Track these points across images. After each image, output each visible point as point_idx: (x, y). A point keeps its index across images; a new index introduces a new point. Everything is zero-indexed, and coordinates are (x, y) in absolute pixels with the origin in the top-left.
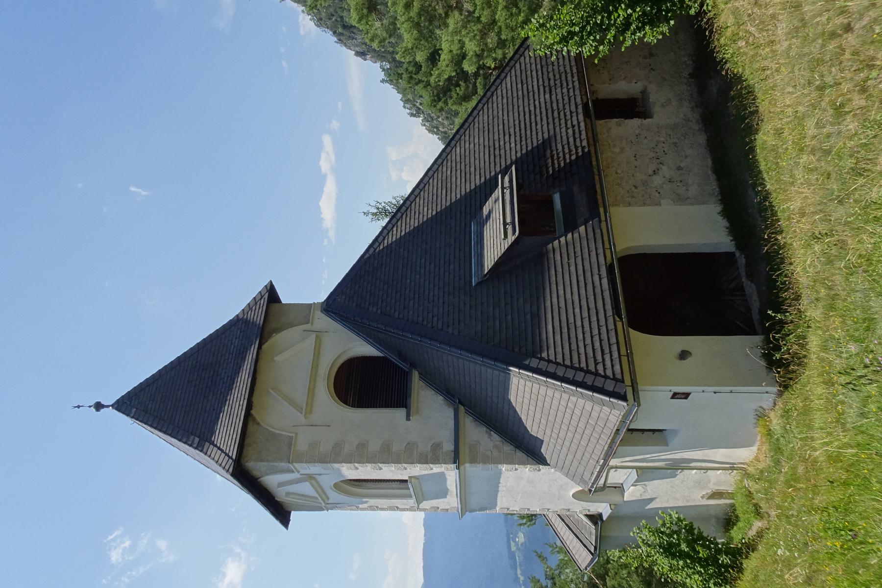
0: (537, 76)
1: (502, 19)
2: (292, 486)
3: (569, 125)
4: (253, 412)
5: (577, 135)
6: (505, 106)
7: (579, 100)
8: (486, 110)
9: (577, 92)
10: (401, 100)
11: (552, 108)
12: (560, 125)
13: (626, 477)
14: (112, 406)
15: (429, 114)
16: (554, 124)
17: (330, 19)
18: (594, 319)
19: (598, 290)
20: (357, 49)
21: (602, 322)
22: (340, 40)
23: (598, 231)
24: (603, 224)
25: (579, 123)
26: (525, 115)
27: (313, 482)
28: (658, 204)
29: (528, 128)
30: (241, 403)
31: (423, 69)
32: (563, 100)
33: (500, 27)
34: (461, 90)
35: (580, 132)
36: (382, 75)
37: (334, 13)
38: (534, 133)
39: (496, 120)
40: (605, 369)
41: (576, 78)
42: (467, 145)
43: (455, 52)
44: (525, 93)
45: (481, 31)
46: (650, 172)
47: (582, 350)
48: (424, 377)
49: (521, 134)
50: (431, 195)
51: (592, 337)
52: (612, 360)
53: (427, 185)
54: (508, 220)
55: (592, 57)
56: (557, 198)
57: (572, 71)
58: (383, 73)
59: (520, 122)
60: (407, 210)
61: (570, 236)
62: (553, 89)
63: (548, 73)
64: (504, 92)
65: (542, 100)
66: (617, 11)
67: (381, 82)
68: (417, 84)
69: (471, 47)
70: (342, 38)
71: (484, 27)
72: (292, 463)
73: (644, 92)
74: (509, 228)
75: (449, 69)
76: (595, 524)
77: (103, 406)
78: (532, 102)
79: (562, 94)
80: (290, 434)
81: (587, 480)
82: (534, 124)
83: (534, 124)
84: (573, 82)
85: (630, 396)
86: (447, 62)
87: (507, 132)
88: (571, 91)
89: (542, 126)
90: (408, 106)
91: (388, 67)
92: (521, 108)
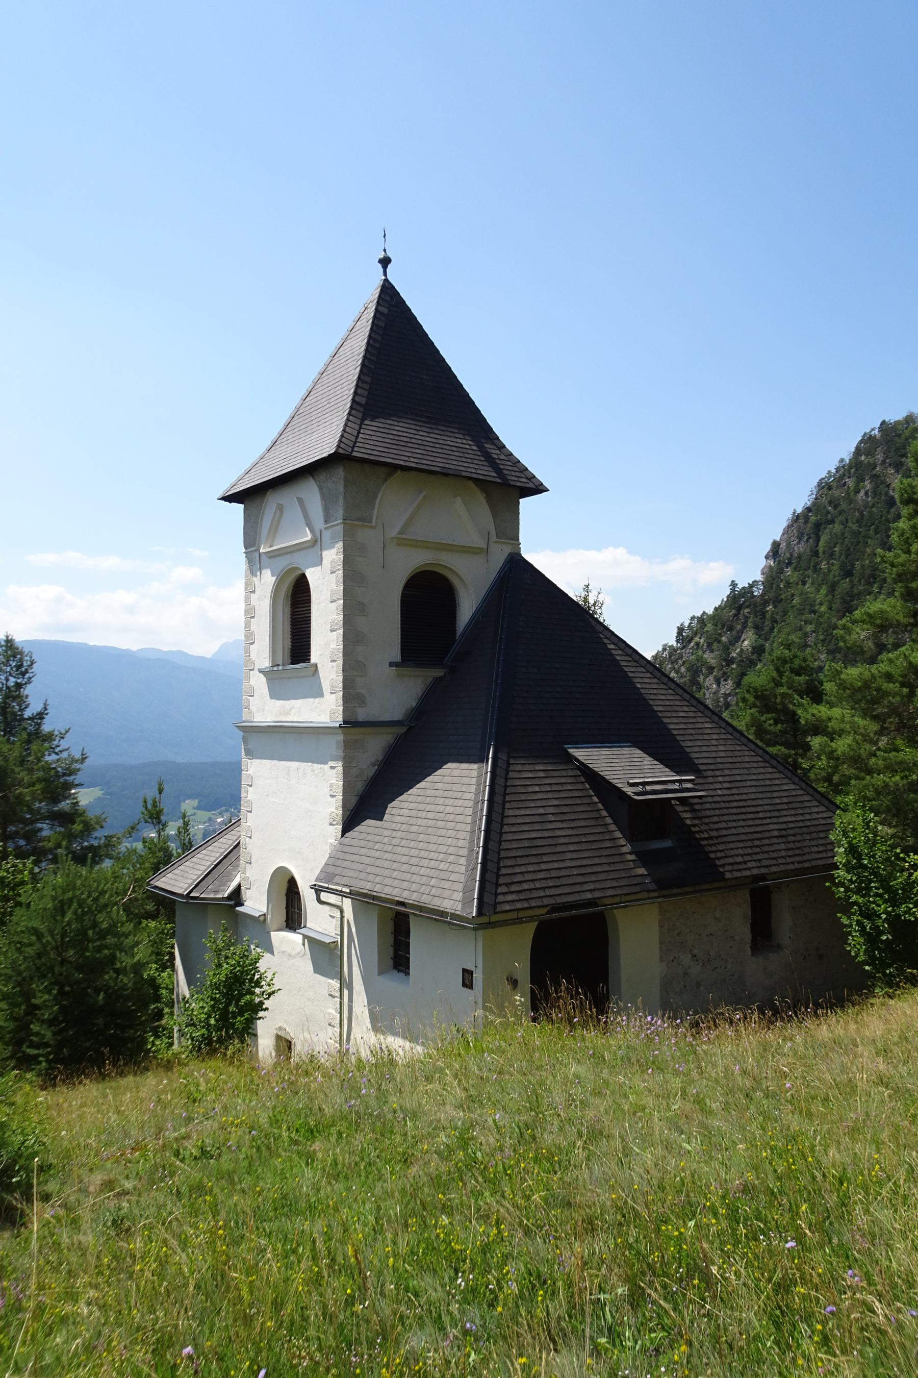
0: (798, 821)
1: (874, 781)
2: (303, 519)
3: (747, 858)
4: (399, 472)
5: (736, 867)
6: (762, 783)
7: (774, 869)
8: (755, 759)
9: (783, 868)
10: (704, 613)
11: (763, 839)
12: (746, 848)
13: (320, 930)
14: (386, 280)
15: (682, 657)
16: (746, 841)
17: (830, 503)
18: (550, 883)
19: (578, 888)
20: (783, 545)
21: (548, 892)
22: (798, 517)
23: (637, 889)
24: (645, 895)
25: (749, 869)
26: (754, 806)
28: (661, 961)
29: (739, 810)
30: (412, 460)
31: (797, 678)
32: (773, 851)
33: (863, 779)
34: (770, 725)
35: (740, 870)
36: (742, 584)
37: (839, 509)
38: (735, 817)
39: (746, 771)
40: (504, 894)
41: (797, 866)
42: (715, 737)
43: (830, 724)
44: (779, 807)
45: (859, 757)
46: (695, 951)
47: (517, 870)
48: (437, 681)
49: (732, 801)
50: (655, 692)
51: (532, 881)
52: (513, 901)
53: (665, 687)
54: (648, 788)
55: (832, 878)
56: (667, 844)
57: (805, 861)
58: (747, 585)
59: (746, 800)
60: (635, 661)
62: (784, 840)
63: (802, 834)
64: (777, 782)
65: (772, 827)
66: (884, 903)
67: (733, 581)
68: (777, 669)
69: (842, 745)
70: (801, 521)
71: (863, 760)
72: (344, 524)
73: (779, 947)
74: (640, 789)
75: (809, 716)
76: (229, 898)
77: (385, 267)
78: (768, 815)
79: (780, 851)
81: (335, 881)
82: (744, 817)
83: (744, 817)
84: (793, 863)
85: (484, 920)
86: (818, 714)
87: (733, 785)
88: (783, 861)
89: (743, 827)
90: (694, 624)
91: (755, 594)
92: (761, 802)
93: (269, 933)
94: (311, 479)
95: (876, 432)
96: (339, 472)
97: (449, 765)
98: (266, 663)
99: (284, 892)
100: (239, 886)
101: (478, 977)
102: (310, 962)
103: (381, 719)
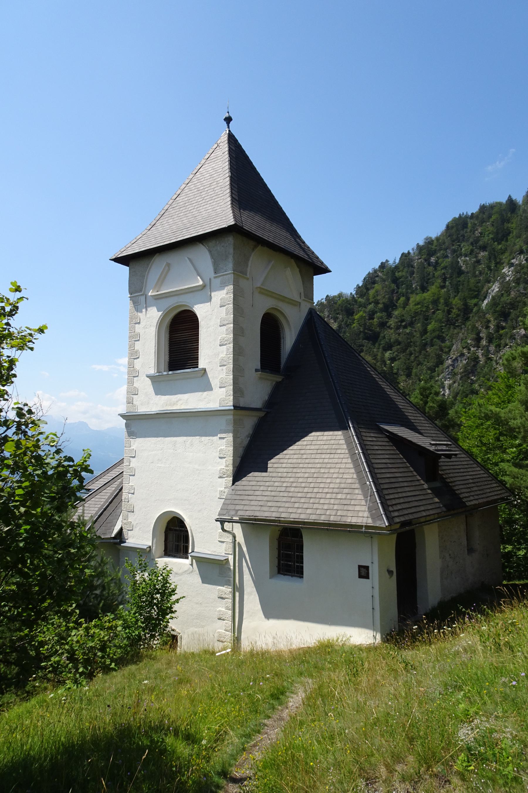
27: (200, 288)
61: (429, 491)
72: (234, 273)
80: (248, 274)
93: (153, 560)
94: (201, 245)
95: (324, 300)
96: (230, 240)
97: (313, 434)
98: (152, 371)
99: (164, 530)
100: (121, 529)
101: (374, 572)
102: (199, 576)
103: (252, 406)
